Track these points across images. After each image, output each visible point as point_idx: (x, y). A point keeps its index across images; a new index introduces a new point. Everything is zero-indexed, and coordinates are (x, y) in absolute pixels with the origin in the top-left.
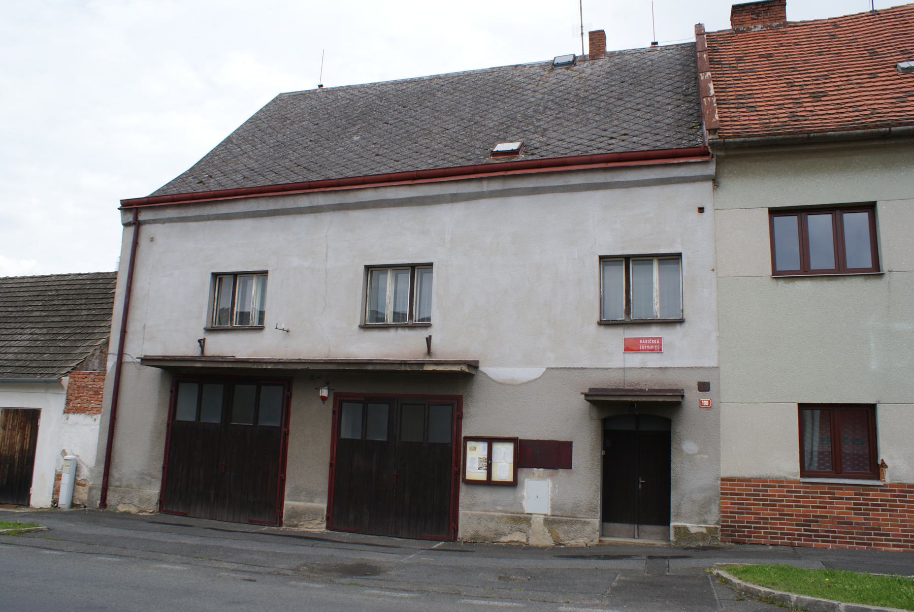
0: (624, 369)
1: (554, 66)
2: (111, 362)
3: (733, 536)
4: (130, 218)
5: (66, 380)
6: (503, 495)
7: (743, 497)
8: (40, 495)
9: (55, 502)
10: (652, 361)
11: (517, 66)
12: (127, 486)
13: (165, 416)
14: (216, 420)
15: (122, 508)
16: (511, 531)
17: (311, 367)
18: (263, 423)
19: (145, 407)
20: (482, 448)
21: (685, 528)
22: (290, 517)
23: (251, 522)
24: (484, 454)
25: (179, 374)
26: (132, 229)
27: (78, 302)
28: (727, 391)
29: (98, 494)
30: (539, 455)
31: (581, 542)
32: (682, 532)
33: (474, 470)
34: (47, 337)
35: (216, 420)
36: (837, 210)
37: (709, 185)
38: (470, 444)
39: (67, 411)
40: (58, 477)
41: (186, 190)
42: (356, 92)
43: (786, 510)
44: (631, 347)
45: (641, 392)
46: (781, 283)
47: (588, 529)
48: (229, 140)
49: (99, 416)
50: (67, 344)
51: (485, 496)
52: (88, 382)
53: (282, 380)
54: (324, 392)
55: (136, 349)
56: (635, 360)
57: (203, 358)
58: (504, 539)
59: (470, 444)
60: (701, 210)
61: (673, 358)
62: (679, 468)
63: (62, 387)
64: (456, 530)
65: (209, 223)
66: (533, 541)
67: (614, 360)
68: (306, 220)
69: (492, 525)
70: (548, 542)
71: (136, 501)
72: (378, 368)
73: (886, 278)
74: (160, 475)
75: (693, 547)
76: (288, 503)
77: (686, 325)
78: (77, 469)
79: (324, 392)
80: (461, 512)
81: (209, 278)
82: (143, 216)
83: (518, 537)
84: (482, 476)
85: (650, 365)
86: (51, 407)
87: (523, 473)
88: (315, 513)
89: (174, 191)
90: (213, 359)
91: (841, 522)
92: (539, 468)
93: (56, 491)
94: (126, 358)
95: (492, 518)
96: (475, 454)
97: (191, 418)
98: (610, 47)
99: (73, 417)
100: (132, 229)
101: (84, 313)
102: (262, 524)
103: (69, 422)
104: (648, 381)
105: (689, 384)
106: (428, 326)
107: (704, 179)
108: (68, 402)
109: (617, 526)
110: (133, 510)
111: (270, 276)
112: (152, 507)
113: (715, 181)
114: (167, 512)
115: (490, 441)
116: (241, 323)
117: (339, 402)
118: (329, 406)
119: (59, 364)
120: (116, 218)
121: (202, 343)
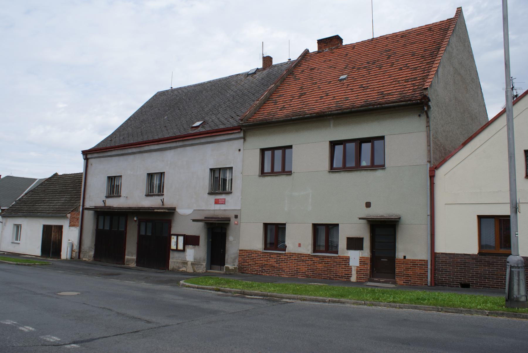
0: (214, 210)
1: (247, 75)
5: (69, 215)
6: (181, 254)
7: (244, 254)
8: (65, 254)
13: (95, 227)
15: (84, 259)
16: (183, 267)
18: (120, 229)
20: (175, 237)
21: (228, 267)
22: (127, 262)
23: (117, 264)
24: (176, 240)
25: (102, 213)
28: (243, 218)
29: (77, 254)
30: (191, 240)
32: (227, 268)
33: (173, 247)
35: (108, 229)
36: (273, 149)
37: (242, 140)
38: (172, 237)
39: (70, 226)
42: (185, 91)
43: (257, 262)
44: (217, 202)
47: (202, 267)
54: (135, 219)
56: (218, 207)
58: (181, 270)
59: (172, 237)
60: (240, 150)
61: (231, 204)
63: (67, 218)
66: (188, 271)
67: (210, 206)
68: (131, 157)
69: (178, 265)
70: (192, 271)
73: (293, 175)
74: (93, 247)
75: (229, 273)
76: (126, 257)
77: (232, 194)
78: (73, 246)
79: (135, 219)
80: (171, 260)
81: (106, 178)
82: (89, 156)
83: (184, 269)
85: (222, 209)
86: (65, 223)
87: (187, 247)
88: (133, 260)
90: (110, 208)
91: (272, 266)
95: (178, 262)
96: (174, 239)
98: (274, 63)
99: (72, 228)
102: (119, 264)
104: (221, 215)
105: (232, 215)
107: (240, 138)
109: (215, 266)
111: (386, 138)
112: (92, 259)
113: (244, 138)
115: (177, 235)
116: (158, 192)
117: (140, 222)
118: (137, 223)
121: (104, 202)
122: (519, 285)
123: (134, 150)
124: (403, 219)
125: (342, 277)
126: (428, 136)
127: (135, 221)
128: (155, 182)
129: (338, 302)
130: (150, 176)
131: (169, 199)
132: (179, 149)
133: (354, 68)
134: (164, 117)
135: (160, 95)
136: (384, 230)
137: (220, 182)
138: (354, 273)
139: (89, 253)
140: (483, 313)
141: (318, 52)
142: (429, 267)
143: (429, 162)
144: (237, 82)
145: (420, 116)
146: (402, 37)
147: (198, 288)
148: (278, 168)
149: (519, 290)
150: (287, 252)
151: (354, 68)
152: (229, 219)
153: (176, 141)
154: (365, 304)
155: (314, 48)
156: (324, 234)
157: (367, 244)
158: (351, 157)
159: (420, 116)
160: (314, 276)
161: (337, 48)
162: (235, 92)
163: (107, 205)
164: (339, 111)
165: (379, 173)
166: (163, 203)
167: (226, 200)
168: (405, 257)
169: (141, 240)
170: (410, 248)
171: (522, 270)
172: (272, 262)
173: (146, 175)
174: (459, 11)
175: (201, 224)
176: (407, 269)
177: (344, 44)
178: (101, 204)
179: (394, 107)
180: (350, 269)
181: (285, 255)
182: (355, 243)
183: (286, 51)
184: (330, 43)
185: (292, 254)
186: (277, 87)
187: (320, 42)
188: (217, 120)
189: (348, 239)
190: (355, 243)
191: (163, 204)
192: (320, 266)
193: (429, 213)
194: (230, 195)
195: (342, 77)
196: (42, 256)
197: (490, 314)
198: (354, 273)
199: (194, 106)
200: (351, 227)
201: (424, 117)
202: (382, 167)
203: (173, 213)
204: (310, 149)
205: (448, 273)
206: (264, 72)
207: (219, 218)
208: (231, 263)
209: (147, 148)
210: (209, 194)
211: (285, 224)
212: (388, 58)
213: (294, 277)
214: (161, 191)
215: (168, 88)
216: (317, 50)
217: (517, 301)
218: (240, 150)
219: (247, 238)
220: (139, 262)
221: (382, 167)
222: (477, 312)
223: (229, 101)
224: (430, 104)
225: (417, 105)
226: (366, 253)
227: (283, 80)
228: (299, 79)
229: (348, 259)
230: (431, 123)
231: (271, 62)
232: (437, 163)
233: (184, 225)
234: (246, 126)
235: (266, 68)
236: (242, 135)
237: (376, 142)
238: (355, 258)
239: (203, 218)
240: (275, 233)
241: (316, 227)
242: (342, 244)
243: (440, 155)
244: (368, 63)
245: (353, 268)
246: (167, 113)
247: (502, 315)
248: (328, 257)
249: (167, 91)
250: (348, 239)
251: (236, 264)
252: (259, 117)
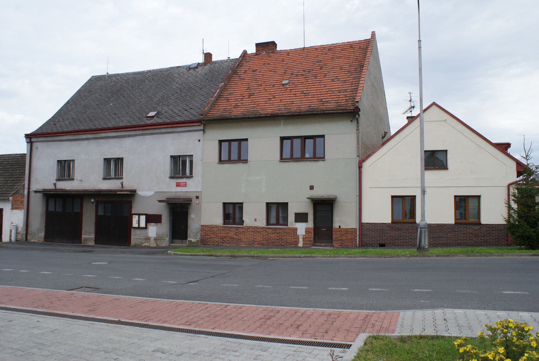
1: (189, 68)
2: (26, 192)
3: (204, 242)
4: (29, 140)
5: (11, 198)
6: (143, 231)
7: (206, 229)
9: (10, 240)
10: (183, 189)
11: (178, 67)
14: (61, 210)
15: (32, 241)
16: (145, 242)
18: (75, 211)
19: (38, 206)
20: (137, 217)
25: (50, 196)
26: (29, 144)
27: (16, 167)
28: (204, 198)
29: (24, 236)
30: (152, 219)
31: (164, 245)
32: (190, 241)
33: (135, 224)
34: (4, 182)
35: (61, 210)
36: (230, 141)
37: (202, 132)
38: (134, 216)
39: (12, 209)
40: (11, 231)
41: (45, 131)
42: (119, 78)
44: (178, 185)
47: (165, 241)
48: (68, 103)
50: (11, 184)
51: (138, 232)
52: (19, 198)
53: (81, 196)
54: (93, 200)
55: (34, 187)
56: (179, 189)
57: (56, 190)
58: (144, 245)
59: (134, 216)
60: (199, 141)
61: (191, 187)
62: (190, 222)
63: (10, 201)
66: (151, 245)
67: (172, 188)
68: (85, 142)
69: (140, 241)
70: (155, 245)
73: (248, 163)
74: (44, 229)
75: (192, 245)
76: (83, 236)
78: (17, 228)
79: (93, 200)
80: (132, 237)
81: (56, 162)
82: (33, 140)
83: (147, 244)
84: (137, 226)
86: (7, 208)
87: (149, 224)
88: (91, 239)
89: (40, 132)
90: (62, 190)
93: (11, 236)
94: (31, 190)
95: (140, 239)
96: (135, 219)
97: (53, 210)
98: (214, 59)
100: (29, 144)
101: (18, 171)
102: (76, 243)
104: (183, 196)
105: (193, 196)
106: (122, 178)
108: (12, 206)
109: (176, 240)
110: (36, 241)
112: (42, 240)
113: (204, 131)
114: (47, 241)
115: (139, 215)
116: (115, 176)
119: (8, 192)
120: (24, 139)
121: (55, 184)
122: (425, 238)
123: (89, 136)
124: (338, 198)
125: (291, 244)
126: (358, 137)
127: (92, 202)
128: (113, 167)
129: (311, 257)
130: (107, 161)
131: (129, 181)
132: (138, 137)
133: (292, 74)
134: (109, 104)
135: (95, 81)
136: (324, 207)
137: (181, 166)
138: (301, 240)
140: (406, 256)
141: (256, 54)
142: (358, 233)
143: (358, 156)
144: (179, 75)
145: (352, 121)
146: (329, 50)
147: (191, 255)
148: (234, 156)
149: (425, 242)
150: (244, 225)
151: (292, 74)
152: (190, 200)
153: (136, 130)
154: (330, 257)
155: (252, 50)
156: (277, 210)
157: (311, 217)
158: (302, 151)
159: (352, 121)
160: (268, 244)
161: (273, 52)
162: (181, 84)
164: (290, 114)
165: (320, 163)
166: (122, 185)
167: (187, 184)
168: (340, 227)
170: (344, 220)
171: (426, 230)
172: (232, 234)
173: (103, 160)
174: (373, 34)
175: (163, 204)
176: (342, 235)
177: (278, 49)
178: (52, 187)
179: (333, 113)
180: (298, 237)
181: (243, 228)
182: (301, 217)
183: (227, 50)
184: (266, 48)
185: (248, 228)
186: (225, 85)
187: (258, 45)
188: (170, 112)
189: (296, 214)
190: (301, 217)
191: (122, 187)
192: (273, 236)
193: (358, 194)
194: (191, 179)
195: (284, 82)
197: (411, 256)
198: (301, 240)
199: (140, 95)
200: (298, 204)
201: (355, 122)
202: (323, 158)
203: (134, 195)
204: (263, 143)
205: (372, 237)
206: (206, 67)
207: (180, 199)
209: (103, 135)
210: (170, 178)
211: (242, 203)
212: (321, 69)
213: (251, 245)
214: (118, 176)
215: (104, 73)
216: (255, 52)
217: (424, 248)
218: (199, 141)
219: (208, 215)
221: (323, 158)
222: (403, 256)
223: (176, 93)
224: (360, 113)
225: (352, 113)
226: (310, 224)
227: (229, 79)
228: (244, 79)
229: (296, 229)
230: (360, 127)
231: (211, 58)
232: (364, 158)
234: (206, 120)
235: (207, 63)
236: (202, 127)
237: (318, 140)
238: (301, 228)
239: (165, 199)
240: (232, 212)
241: (269, 205)
242: (291, 218)
243: (365, 153)
244: (304, 71)
245: (300, 236)
246: (111, 100)
247: (417, 256)
248: (280, 229)
249: (103, 76)
250: (296, 214)
252: (217, 113)
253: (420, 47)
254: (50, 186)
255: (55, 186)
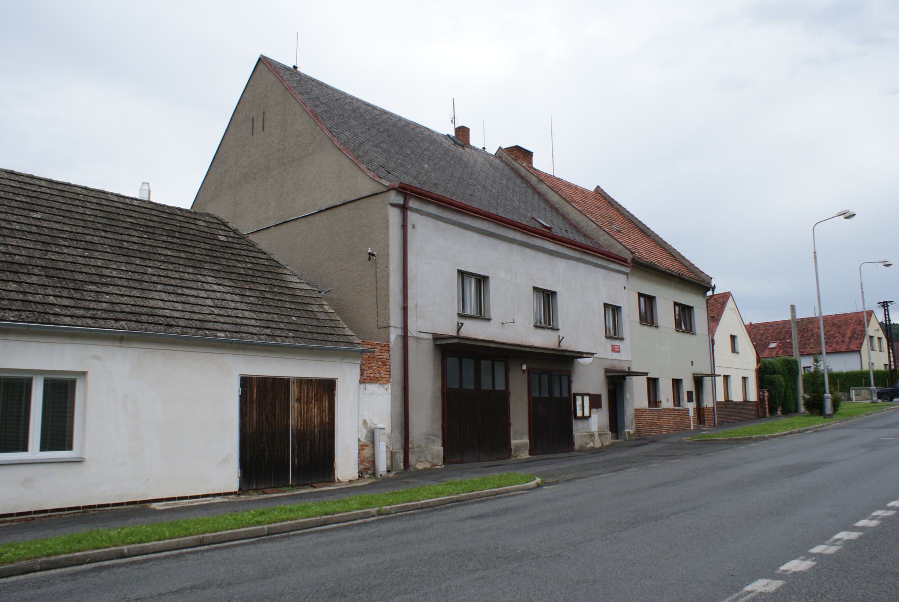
8: (346, 466)
12: (418, 447)
13: (439, 384)
14: (472, 387)
15: (420, 466)
17: (546, 352)
18: (497, 388)
22: (515, 451)
23: (498, 459)
25: (452, 351)
33: (579, 414)
35: (547, 395)
45: (109, 343)
46: (645, 328)
49: (389, 386)
56: (615, 356)
64: (574, 444)
65: (452, 227)
69: (585, 440)
71: (429, 458)
72: (507, 347)
76: (512, 442)
79: (524, 367)
83: (591, 445)
86: (346, 376)
88: (523, 445)
92: (443, 445)
99: (371, 388)
103: (367, 392)
112: (440, 462)
114: (449, 463)
115: (583, 395)
127: (524, 371)
139: (430, 450)
163: (464, 332)
169: (534, 404)
179: (571, 244)
196: (242, 491)
208: (630, 429)
209: (538, 242)
220: (534, 449)
233: (588, 380)
251: (634, 427)
253: (815, 258)
254: (449, 329)
255: (459, 330)
